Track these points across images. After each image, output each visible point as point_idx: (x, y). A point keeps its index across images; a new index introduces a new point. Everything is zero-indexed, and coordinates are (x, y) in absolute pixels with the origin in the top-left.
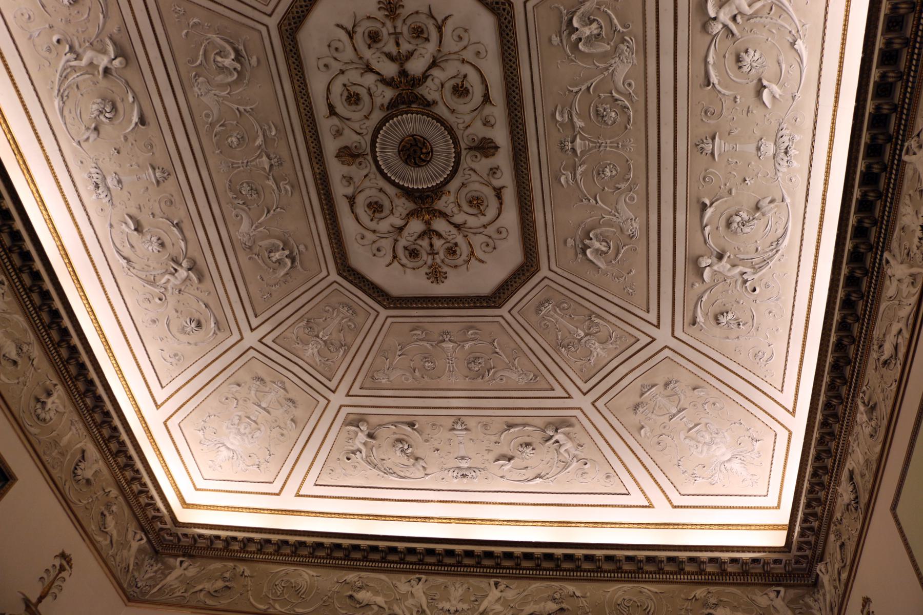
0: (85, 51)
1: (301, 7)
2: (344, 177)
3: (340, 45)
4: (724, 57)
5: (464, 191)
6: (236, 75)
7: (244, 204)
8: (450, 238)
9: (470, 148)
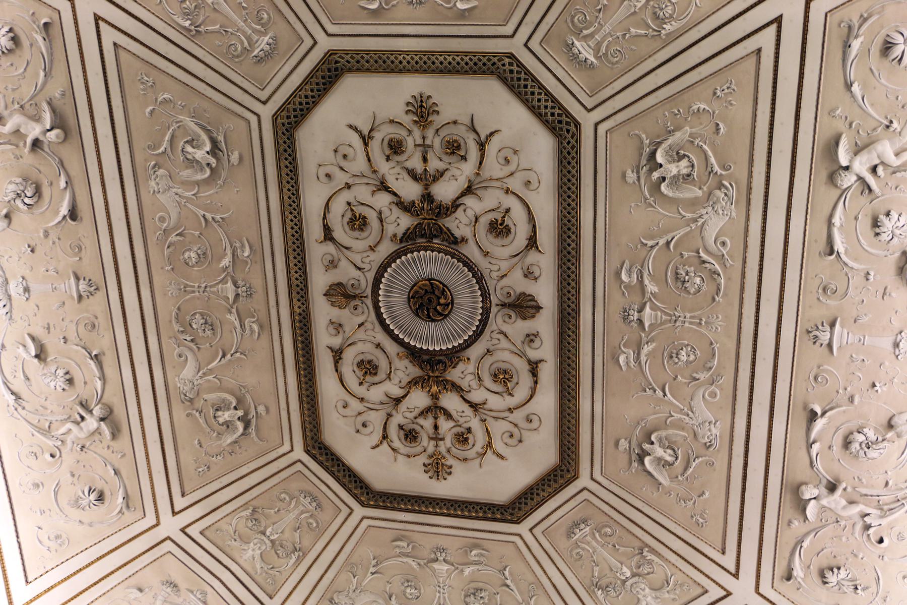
0: (11, 115)
1: (306, 97)
2: (331, 323)
3: (349, 152)
4: (856, 218)
5: (489, 360)
6: (208, 172)
7: (192, 341)
8: (462, 420)
9: (504, 305)
